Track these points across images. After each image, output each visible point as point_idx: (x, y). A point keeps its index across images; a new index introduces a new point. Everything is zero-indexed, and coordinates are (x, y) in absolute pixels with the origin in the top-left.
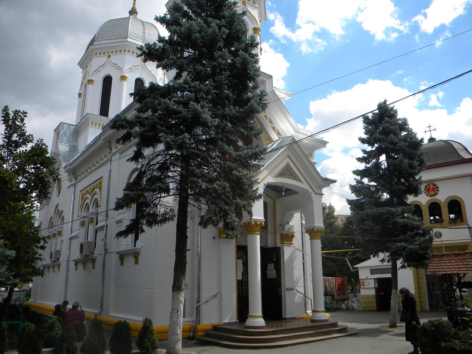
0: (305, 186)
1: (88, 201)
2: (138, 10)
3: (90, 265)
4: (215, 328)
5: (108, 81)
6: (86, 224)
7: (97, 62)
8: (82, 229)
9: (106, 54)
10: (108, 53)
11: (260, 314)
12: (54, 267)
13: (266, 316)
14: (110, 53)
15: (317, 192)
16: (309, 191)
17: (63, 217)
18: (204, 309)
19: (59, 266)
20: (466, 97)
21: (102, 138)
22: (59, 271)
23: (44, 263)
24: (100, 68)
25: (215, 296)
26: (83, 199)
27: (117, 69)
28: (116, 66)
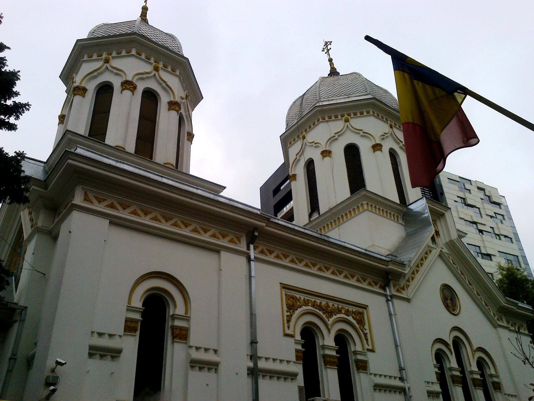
24: (336, 137)
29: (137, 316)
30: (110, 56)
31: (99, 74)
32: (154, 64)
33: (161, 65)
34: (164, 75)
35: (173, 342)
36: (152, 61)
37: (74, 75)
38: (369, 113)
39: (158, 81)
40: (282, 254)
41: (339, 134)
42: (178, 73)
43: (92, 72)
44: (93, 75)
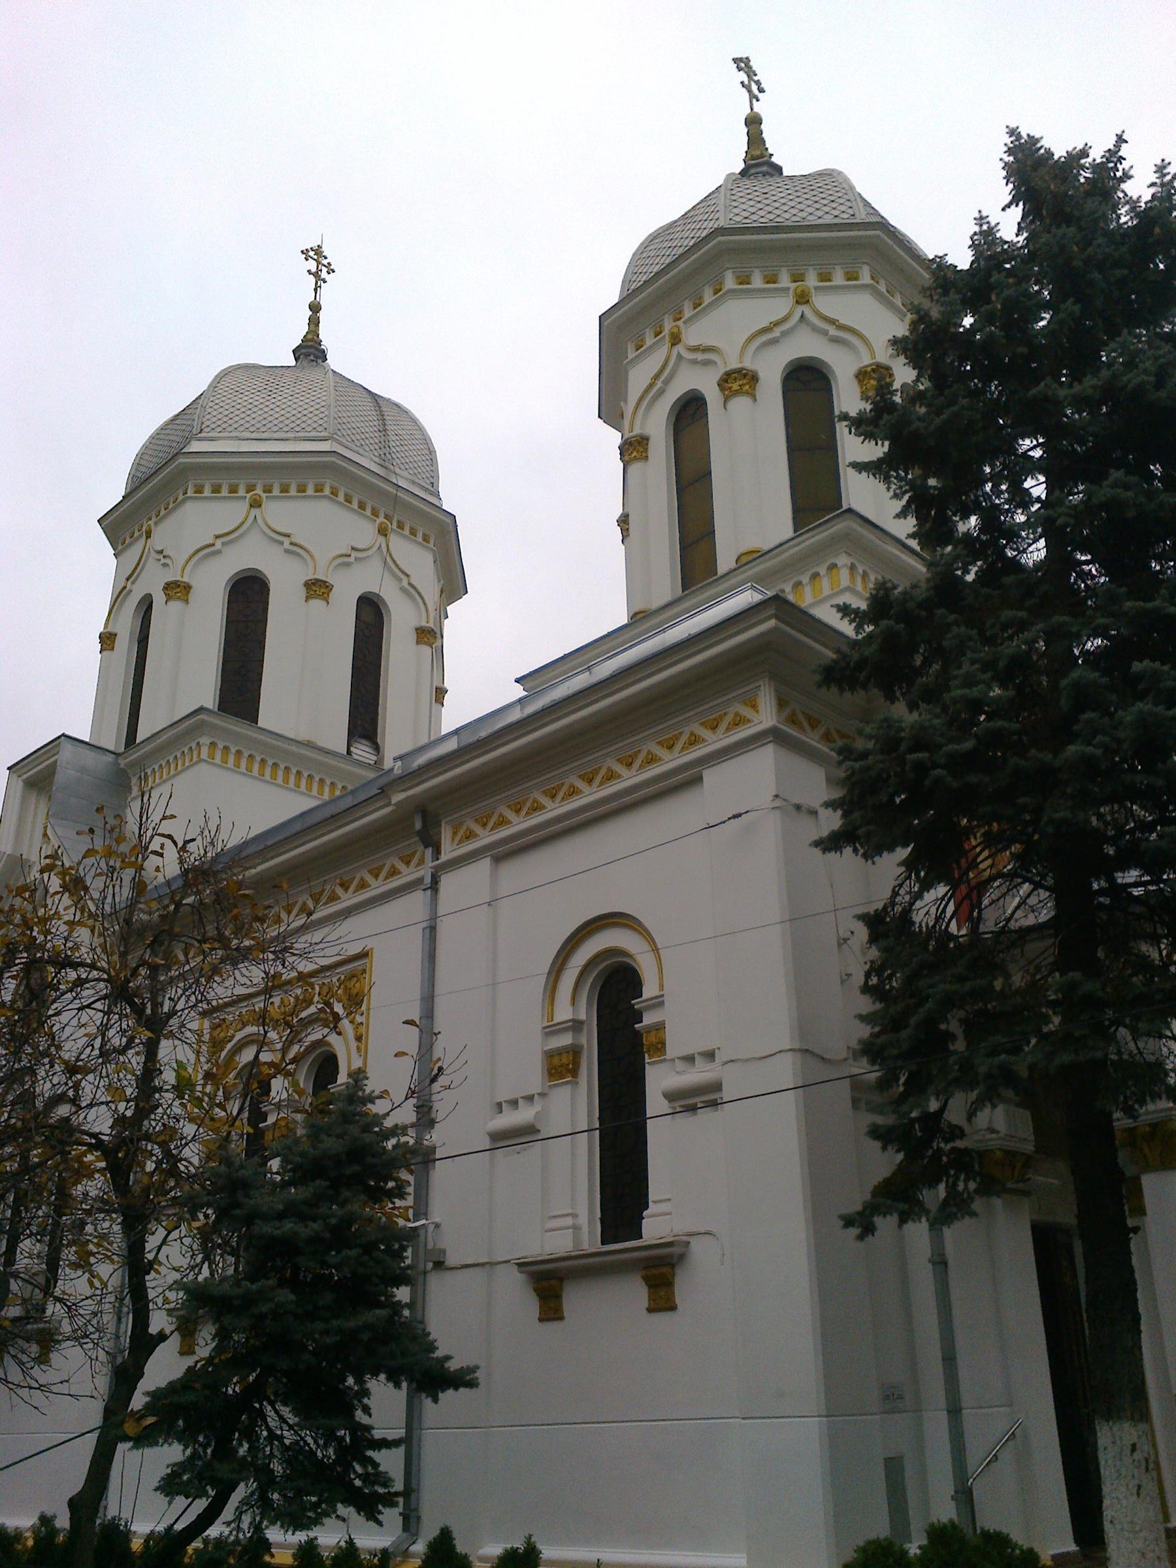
5: (248, 597)
7: (195, 522)
9: (242, 492)
14: (259, 491)
20: (1057, 906)
24: (219, 543)
27: (287, 551)
28: (286, 541)
29: (1130, 1223)
30: (680, 323)
31: (667, 382)
33: (812, 281)
34: (827, 304)
36: (785, 281)
37: (622, 404)
38: (322, 490)
39: (815, 329)
40: (803, 713)
41: (228, 537)
42: (866, 278)
43: (651, 386)
44: (656, 388)
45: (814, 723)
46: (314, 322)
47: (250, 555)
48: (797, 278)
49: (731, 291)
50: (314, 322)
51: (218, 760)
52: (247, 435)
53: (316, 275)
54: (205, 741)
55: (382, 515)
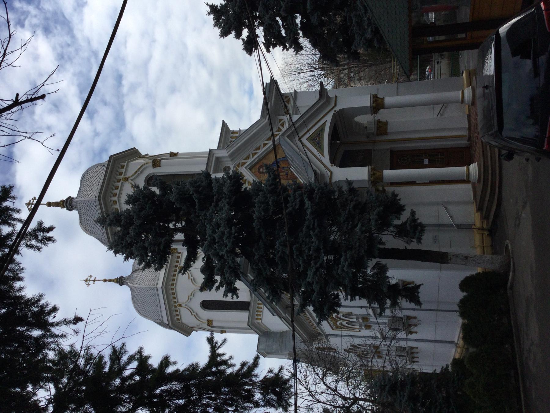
0: (329, 118)
1: (344, 323)
2: (118, 276)
3: (413, 321)
4: (479, 209)
6: (368, 324)
7: (186, 318)
8: (373, 327)
9: (177, 309)
10: (176, 307)
11: (464, 168)
12: (412, 353)
13: (467, 163)
14: (176, 305)
15: (333, 105)
16: (334, 114)
17: (358, 345)
18: (460, 220)
19: (412, 348)
21: (284, 315)
22: (417, 348)
23: (232, 169)
25: (446, 208)
26: (342, 327)
32: (121, 181)
33: (121, 177)
35: (386, 133)
36: (119, 184)
41: (192, 311)
45: (286, 107)
46: (110, 281)
47: (196, 305)
48: (119, 181)
49: (118, 198)
50: (110, 281)
51: (260, 317)
52: (159, 309)
53: (94, 281)
54: (256, 321)
55: (175, 273)
